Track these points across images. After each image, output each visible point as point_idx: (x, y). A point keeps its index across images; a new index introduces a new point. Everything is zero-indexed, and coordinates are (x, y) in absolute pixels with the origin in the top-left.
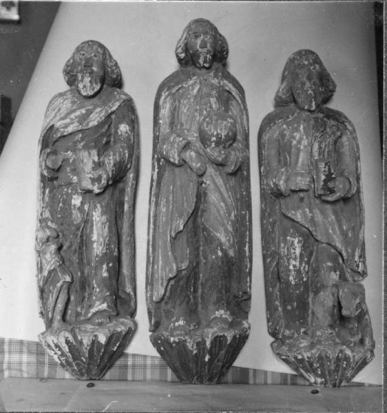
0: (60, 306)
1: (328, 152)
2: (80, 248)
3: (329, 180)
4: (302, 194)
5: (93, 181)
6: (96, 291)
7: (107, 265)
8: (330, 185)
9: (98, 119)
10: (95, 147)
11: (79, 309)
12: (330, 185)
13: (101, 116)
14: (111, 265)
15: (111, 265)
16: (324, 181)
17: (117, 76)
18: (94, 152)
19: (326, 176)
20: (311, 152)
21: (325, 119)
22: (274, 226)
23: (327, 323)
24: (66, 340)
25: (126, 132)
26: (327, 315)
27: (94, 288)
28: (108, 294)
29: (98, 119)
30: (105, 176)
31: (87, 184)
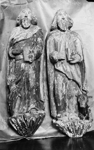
0: (17, 106)
1: (72, 45)
2: (24, 84)
3: (73, 55)
4: (62, 61)
5: (29, 57)
6: (31, 100)
7: (35, 90)
8: (73, 57)
9: (30, 36)
10: (30, 45)
11: (24, 108)
12: (73, 57)
13: (31, 35)
14: (36, 90)
15: (36, 90)
16: (71, 55)
17: (36, 21)
18: (29, 47)
19: (71, 53)
20: (65, 46)
21: (70, 34)
22: (52, 74)
23: (74, 111)
24: (20, 120)
25: (40, 41)
26: (74, 107)
27: (30, 99)
28: (35, 101)
29: (30, 36)
30: (34, 56)
31: (27, 59)
